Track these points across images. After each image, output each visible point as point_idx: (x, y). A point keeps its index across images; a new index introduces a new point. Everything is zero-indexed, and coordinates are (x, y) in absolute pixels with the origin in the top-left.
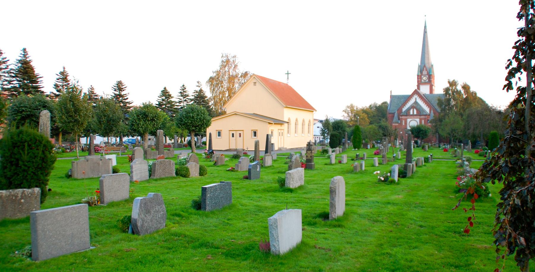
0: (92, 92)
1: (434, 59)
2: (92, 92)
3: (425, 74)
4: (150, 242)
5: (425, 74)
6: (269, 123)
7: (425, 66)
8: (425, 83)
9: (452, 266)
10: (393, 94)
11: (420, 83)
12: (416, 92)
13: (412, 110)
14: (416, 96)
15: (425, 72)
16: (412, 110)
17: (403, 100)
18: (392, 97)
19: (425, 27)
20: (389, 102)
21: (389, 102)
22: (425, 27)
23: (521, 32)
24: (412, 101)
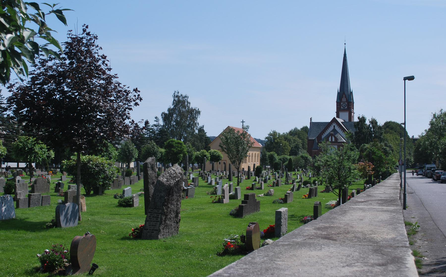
0: (181, 114)
1: (353, 85)
2: (181, 114)
3: (345, 100)
4: (403, 153)
5: (345, 100)
6: (444, 258)
7: (344, 93)
8: (344, 110)
9: (319, 237)
10: (313, 121)
11: (339, 110)
12: (334, 120)
13: (330, 137)
14: (334, 124)
15: (344, 100)
16: (330, 137)
17: (322, 128)
18: (312, 123)
19: (345, 55)
20: (309, 127)
21: (309, 127)
22: (345, 55)
23: (374, 122)
24: (331, 128)
